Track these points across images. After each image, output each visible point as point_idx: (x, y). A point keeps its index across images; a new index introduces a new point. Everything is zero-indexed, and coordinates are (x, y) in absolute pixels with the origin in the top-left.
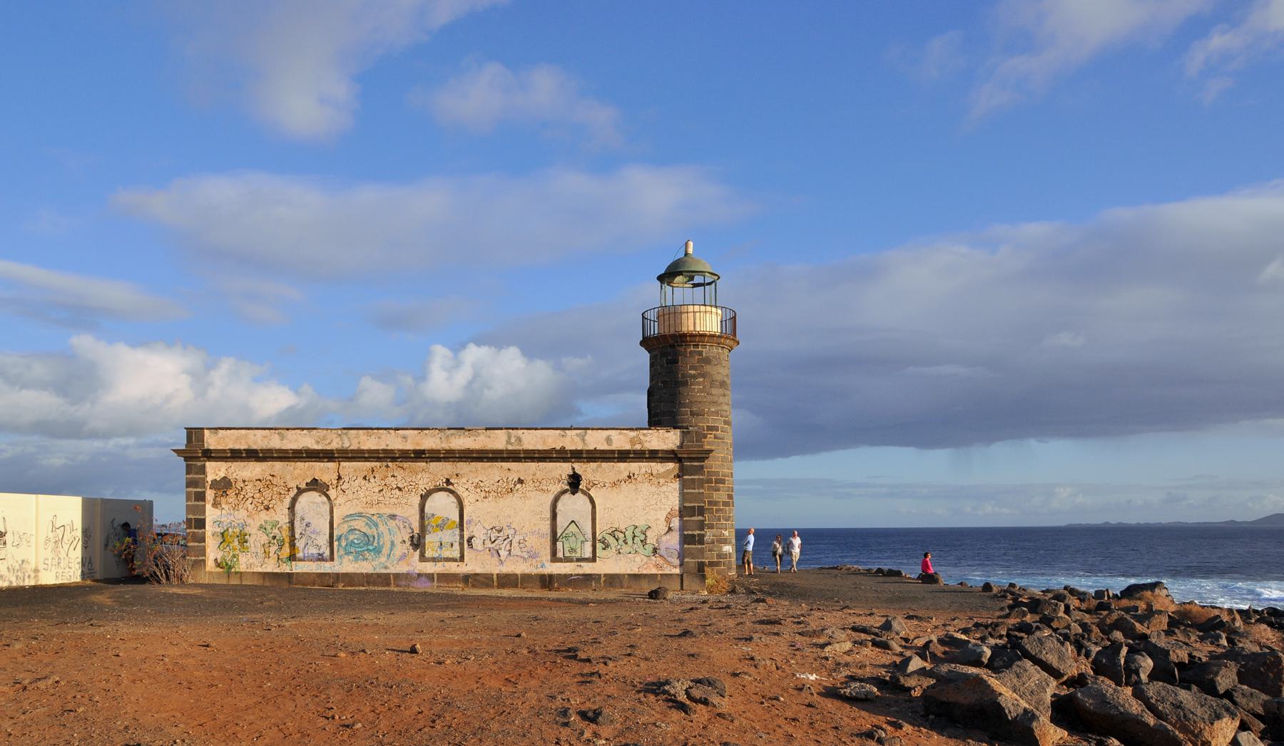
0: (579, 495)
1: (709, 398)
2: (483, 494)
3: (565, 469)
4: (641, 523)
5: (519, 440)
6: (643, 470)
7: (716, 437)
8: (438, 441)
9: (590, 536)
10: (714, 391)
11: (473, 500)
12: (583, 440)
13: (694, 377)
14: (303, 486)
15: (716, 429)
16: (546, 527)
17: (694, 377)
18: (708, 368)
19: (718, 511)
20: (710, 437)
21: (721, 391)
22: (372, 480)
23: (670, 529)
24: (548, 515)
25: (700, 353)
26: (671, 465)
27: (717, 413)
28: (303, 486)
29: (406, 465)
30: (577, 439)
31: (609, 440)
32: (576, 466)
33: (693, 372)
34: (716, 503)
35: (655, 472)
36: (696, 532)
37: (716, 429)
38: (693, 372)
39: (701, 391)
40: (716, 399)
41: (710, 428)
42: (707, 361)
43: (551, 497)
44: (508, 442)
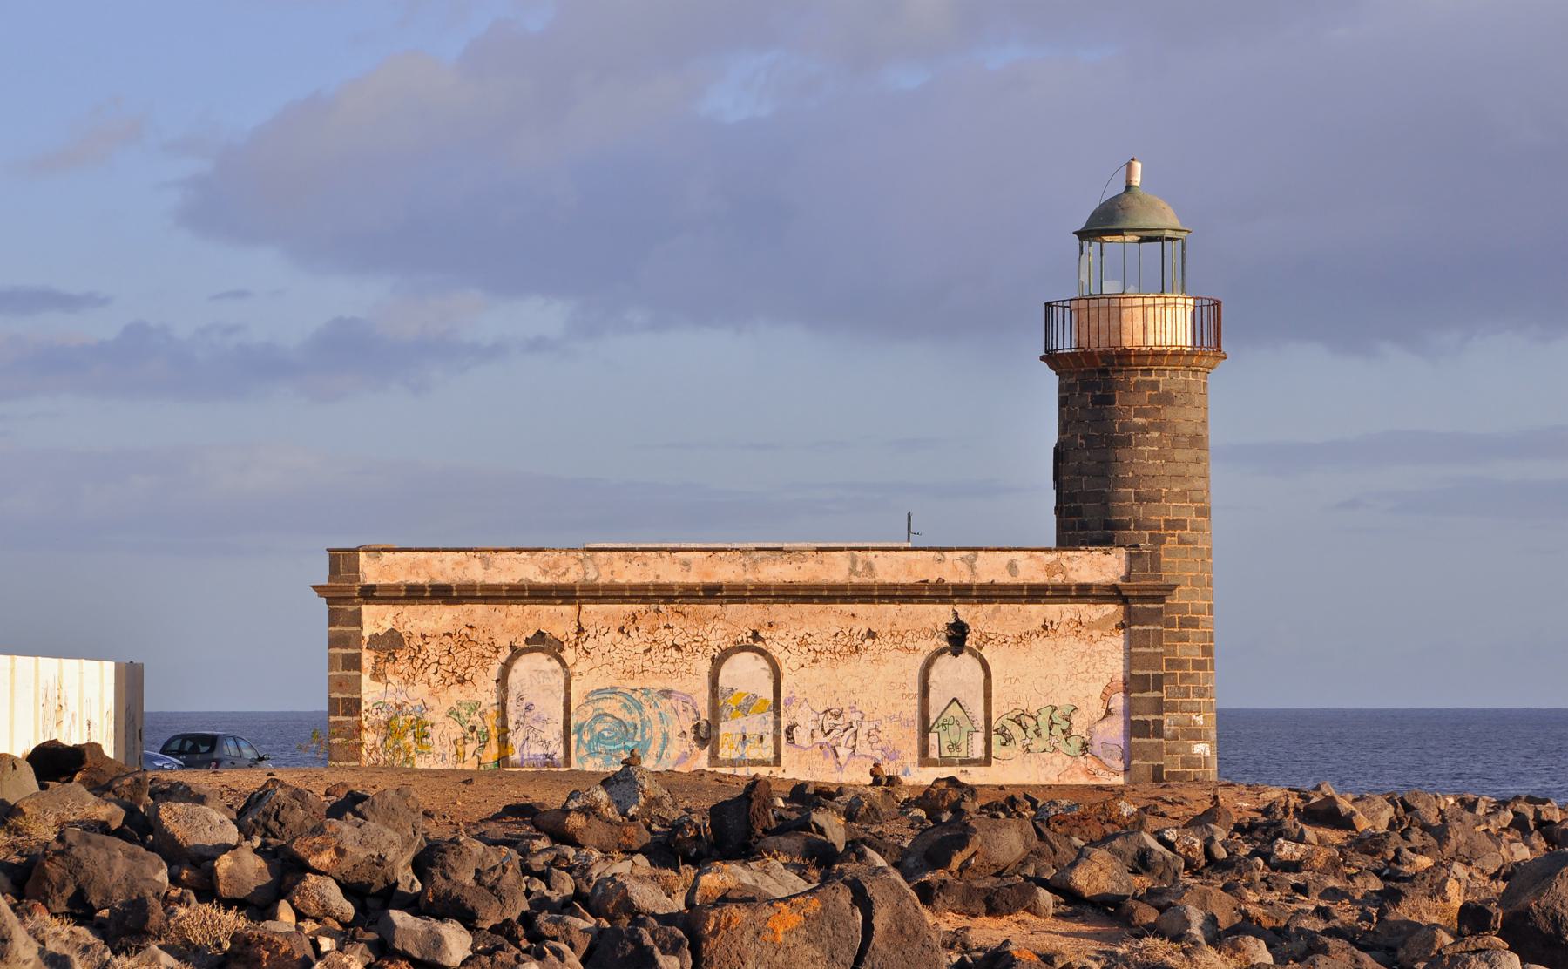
0: (965, 656)
1: (1171, 469)
2: (812, 655)
3: (941, 614)
4: (1063, 702)
5: (869, 567)
6: (1067, 617)
7: (1181, 541)
8: (740, 570)
9: (981, 723)
10: (1179, 455)
11: (795, 666)
12: (972, 568)
13: (1143, 429)
14: (521, 644)
15: (1181, 525)
16: (911, 709)
17: (1143, 429)
18: (1168, 413)
19: (1184, 678)
20: (1171, 542)
21: (1191, 454)
22: (633, 634)
23: (1109, 712)
24: (915, 689)
25: (1155, 385)
26: (1110, 609)
27: (1183, 495)
28: (521, 644)
29: (688, 608)
30: (962, 566)
31: (1012, 568)
32: (960, 609)
33: (1140, 421)
34: (1180, 664)
35: (1085, 619)
36: (1151, 718)
37: (1181, 525)
38: (1140, 421)
39: (1156, 456)
40: (1181, 469)
41: (1170, 525)
42: (1167, 399)
43: (920, 660)
44: (852, 571)
